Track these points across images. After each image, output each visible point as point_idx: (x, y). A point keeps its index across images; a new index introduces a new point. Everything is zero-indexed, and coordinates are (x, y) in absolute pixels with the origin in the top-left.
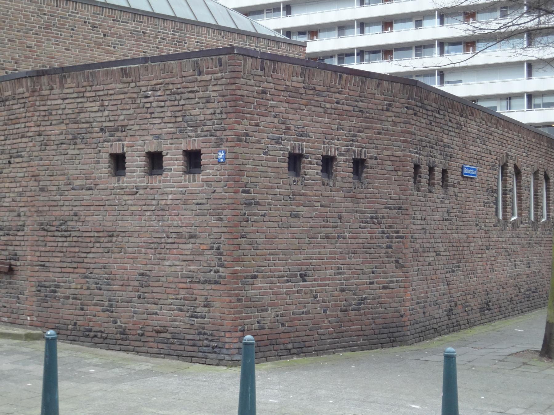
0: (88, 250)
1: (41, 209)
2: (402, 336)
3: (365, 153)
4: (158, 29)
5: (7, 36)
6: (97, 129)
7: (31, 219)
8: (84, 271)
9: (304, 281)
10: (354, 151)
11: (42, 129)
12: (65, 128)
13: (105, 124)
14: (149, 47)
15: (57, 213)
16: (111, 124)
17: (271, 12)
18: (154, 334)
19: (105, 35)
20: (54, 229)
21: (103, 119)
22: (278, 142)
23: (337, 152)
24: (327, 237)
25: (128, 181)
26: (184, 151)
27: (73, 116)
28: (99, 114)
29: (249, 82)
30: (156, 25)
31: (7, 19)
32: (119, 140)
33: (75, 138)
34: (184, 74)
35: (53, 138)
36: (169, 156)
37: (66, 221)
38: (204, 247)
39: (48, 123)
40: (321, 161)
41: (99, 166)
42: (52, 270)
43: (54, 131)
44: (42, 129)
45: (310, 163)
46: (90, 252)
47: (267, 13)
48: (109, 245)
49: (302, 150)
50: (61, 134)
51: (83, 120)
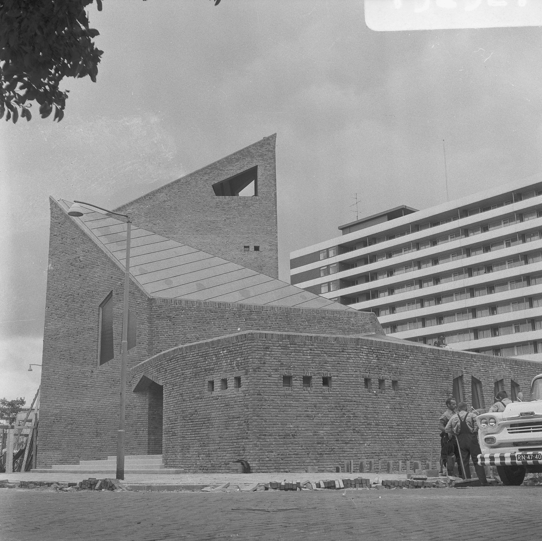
0: (200, 427)
1: (183, 409)
2: (196, 424)
3: (330, 374)
4: (277, 313)
5: (193, 325)
6: (204, 370)
7: (180, 415)
8: (199, 438)
9: (294, 438)
10: (323, 373)
11: (184, 371)
12: (192, 370)
13: (206, 367)
14: (273, 323)
15: (189, 411)
16: (208, 367)
17: (512, 263)
18: (225, 465)
19: (246, 320)
20: (188, 419)
21: (205, 365)
22: (276, 370)
23: (312, 374)
24: (308, 416)
25: (215, 394)
26: (235, 377)
27: (195, 365)
28: (204, 363)
29: (258, 344)
30: (276, 311)
31: (192, 317)
32: (212, 375)
33: (196, 375)
34: (233, 342)
35: (188, 375)
36: (229, 380)
37: (192, 415)
38: (242, 422)
39: (186, 369)
40: (303, 378)
41: (204, 387)
42: (187, 439)
43: (188, 372)
44: (184, 371)
45: (296, 380)
46: (201, 429)
47: (454, 276)
48: (208, 424)
49: (291, 374)
50: (191, 373)
51: (198, 366)
